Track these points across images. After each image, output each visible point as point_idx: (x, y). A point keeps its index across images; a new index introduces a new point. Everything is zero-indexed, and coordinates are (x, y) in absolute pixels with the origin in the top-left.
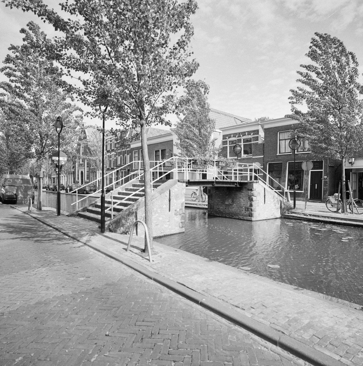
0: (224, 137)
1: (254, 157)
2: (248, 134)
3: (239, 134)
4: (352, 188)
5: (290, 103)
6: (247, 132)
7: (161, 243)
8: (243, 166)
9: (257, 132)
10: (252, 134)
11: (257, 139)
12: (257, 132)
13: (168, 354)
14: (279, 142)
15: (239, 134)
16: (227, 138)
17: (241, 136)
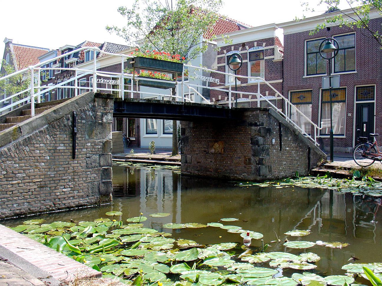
6: (256, 41)
7: (11, 226)
8: (250, 97)
10: (264, 44)
13: (279, 272)
14: (307, 56)
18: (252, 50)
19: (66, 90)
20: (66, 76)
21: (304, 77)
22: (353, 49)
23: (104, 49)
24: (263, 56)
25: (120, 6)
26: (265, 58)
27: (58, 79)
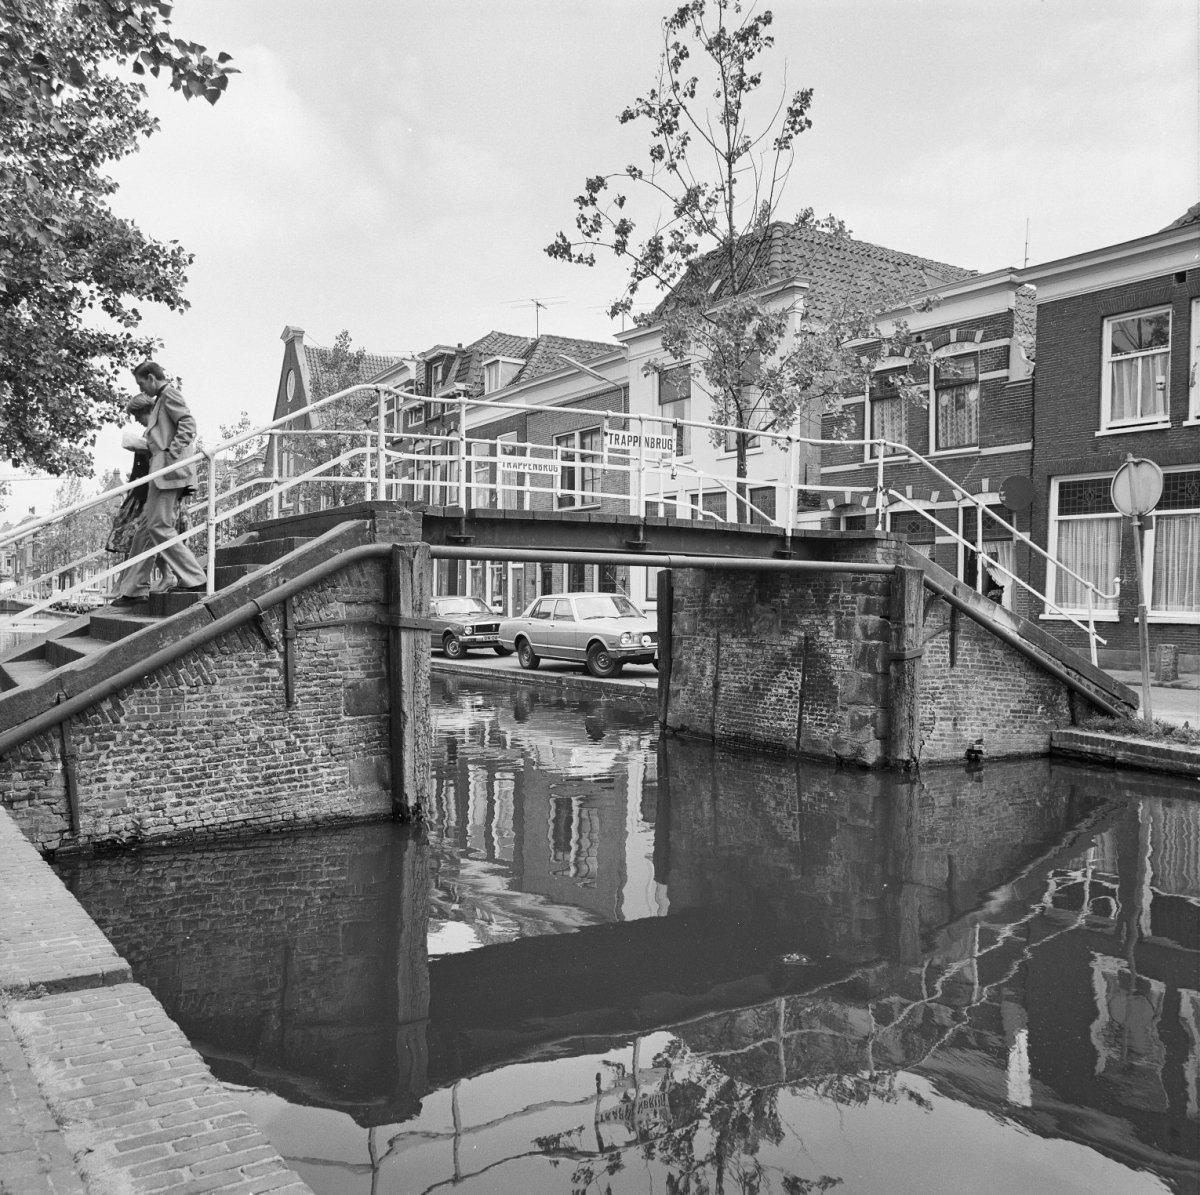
1: (986, 452)
3: (919, 339)
4: (459, 470)
5: (116, 473)
6: (953, 326)
11: (1003, 358)
19: (1127, 408)
21: (1097, 434)
23: (537, 356)
24: (977, 370)
25: (295, 325)
26: (982, 377)
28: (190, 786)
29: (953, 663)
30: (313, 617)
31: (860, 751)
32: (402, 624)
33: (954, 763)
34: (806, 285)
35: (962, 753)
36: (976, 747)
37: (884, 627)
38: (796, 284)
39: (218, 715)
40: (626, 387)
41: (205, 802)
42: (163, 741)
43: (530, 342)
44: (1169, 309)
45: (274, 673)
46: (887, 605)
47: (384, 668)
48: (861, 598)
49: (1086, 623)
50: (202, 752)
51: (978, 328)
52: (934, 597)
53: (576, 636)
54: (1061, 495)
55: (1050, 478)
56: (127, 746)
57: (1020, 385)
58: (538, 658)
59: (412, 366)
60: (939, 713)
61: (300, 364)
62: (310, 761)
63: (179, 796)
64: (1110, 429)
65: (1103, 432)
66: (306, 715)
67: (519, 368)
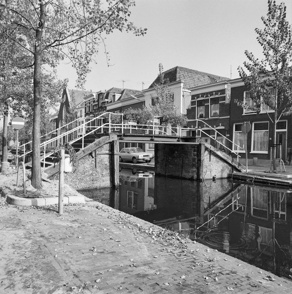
0: (193, 97)
1: (221, 118)
2: (216, 94)
3: (207, 94)
6: (214, 91)
9: (223, 91)
10: (219, 93)
11: (224, 98)
12: (223, 91)
15: (207, 94)
16: (196, 98)
17: (209, 95)
18: (212, 97)
20: (101, 111)
21: (243, 115)
22: (156, 131)
27: (96, 112)
28: (80, 181)
29: (210, 161)
30: (100, 153)
31: (193, 177)
32: (115, 154)
33: (211, 179)
34: (183, 81)
35: (212, 178)
36: (214, 177)
37: (197, 154)
38: (181, 81)
39: (85, 169)
40: (144, 102)
41: (83, 184)
42: (76, 174)
43: (122, 90)
44: (128, 191)
45: (93, 162)
46: (198, 150)
47: (111, 161)
48: (193, 149)
49: (237, 153)
50: (82, 175)
51: (219, 92)
52: (206, 149)
53: (131, 156)
54: (236, 127)
55: (233, 123)
56: (71, 174)
57: (227, 104)
58: (123, 160)
59: (95, 95)
60: (208, 170)
61: (67, 93)
62: (99, 177)
63: (79, 183)
64: (246, 113)
65: (244, 114)
66: (98, 169)
67: (120, 96)
